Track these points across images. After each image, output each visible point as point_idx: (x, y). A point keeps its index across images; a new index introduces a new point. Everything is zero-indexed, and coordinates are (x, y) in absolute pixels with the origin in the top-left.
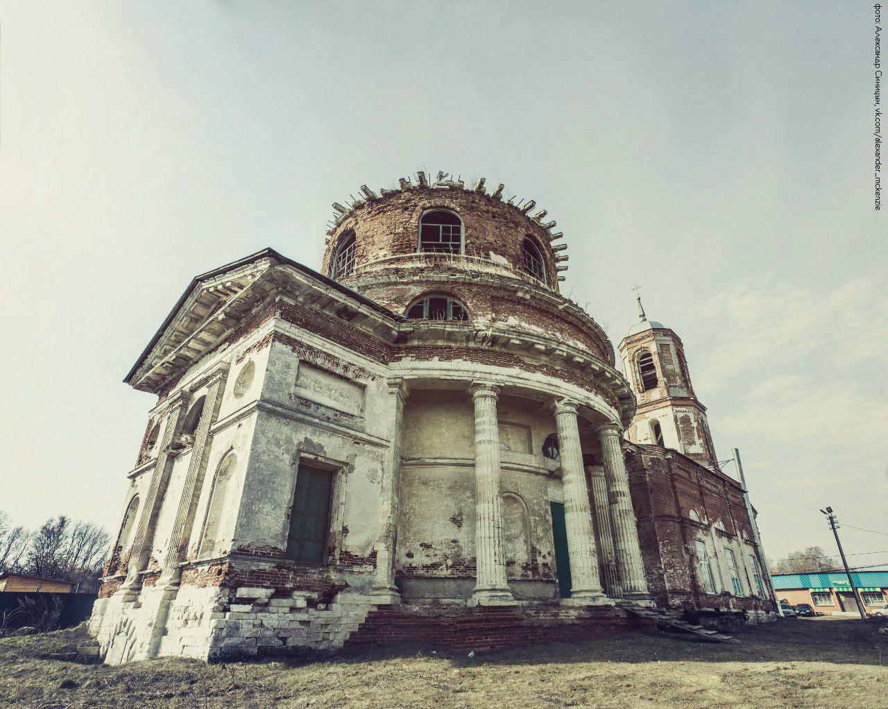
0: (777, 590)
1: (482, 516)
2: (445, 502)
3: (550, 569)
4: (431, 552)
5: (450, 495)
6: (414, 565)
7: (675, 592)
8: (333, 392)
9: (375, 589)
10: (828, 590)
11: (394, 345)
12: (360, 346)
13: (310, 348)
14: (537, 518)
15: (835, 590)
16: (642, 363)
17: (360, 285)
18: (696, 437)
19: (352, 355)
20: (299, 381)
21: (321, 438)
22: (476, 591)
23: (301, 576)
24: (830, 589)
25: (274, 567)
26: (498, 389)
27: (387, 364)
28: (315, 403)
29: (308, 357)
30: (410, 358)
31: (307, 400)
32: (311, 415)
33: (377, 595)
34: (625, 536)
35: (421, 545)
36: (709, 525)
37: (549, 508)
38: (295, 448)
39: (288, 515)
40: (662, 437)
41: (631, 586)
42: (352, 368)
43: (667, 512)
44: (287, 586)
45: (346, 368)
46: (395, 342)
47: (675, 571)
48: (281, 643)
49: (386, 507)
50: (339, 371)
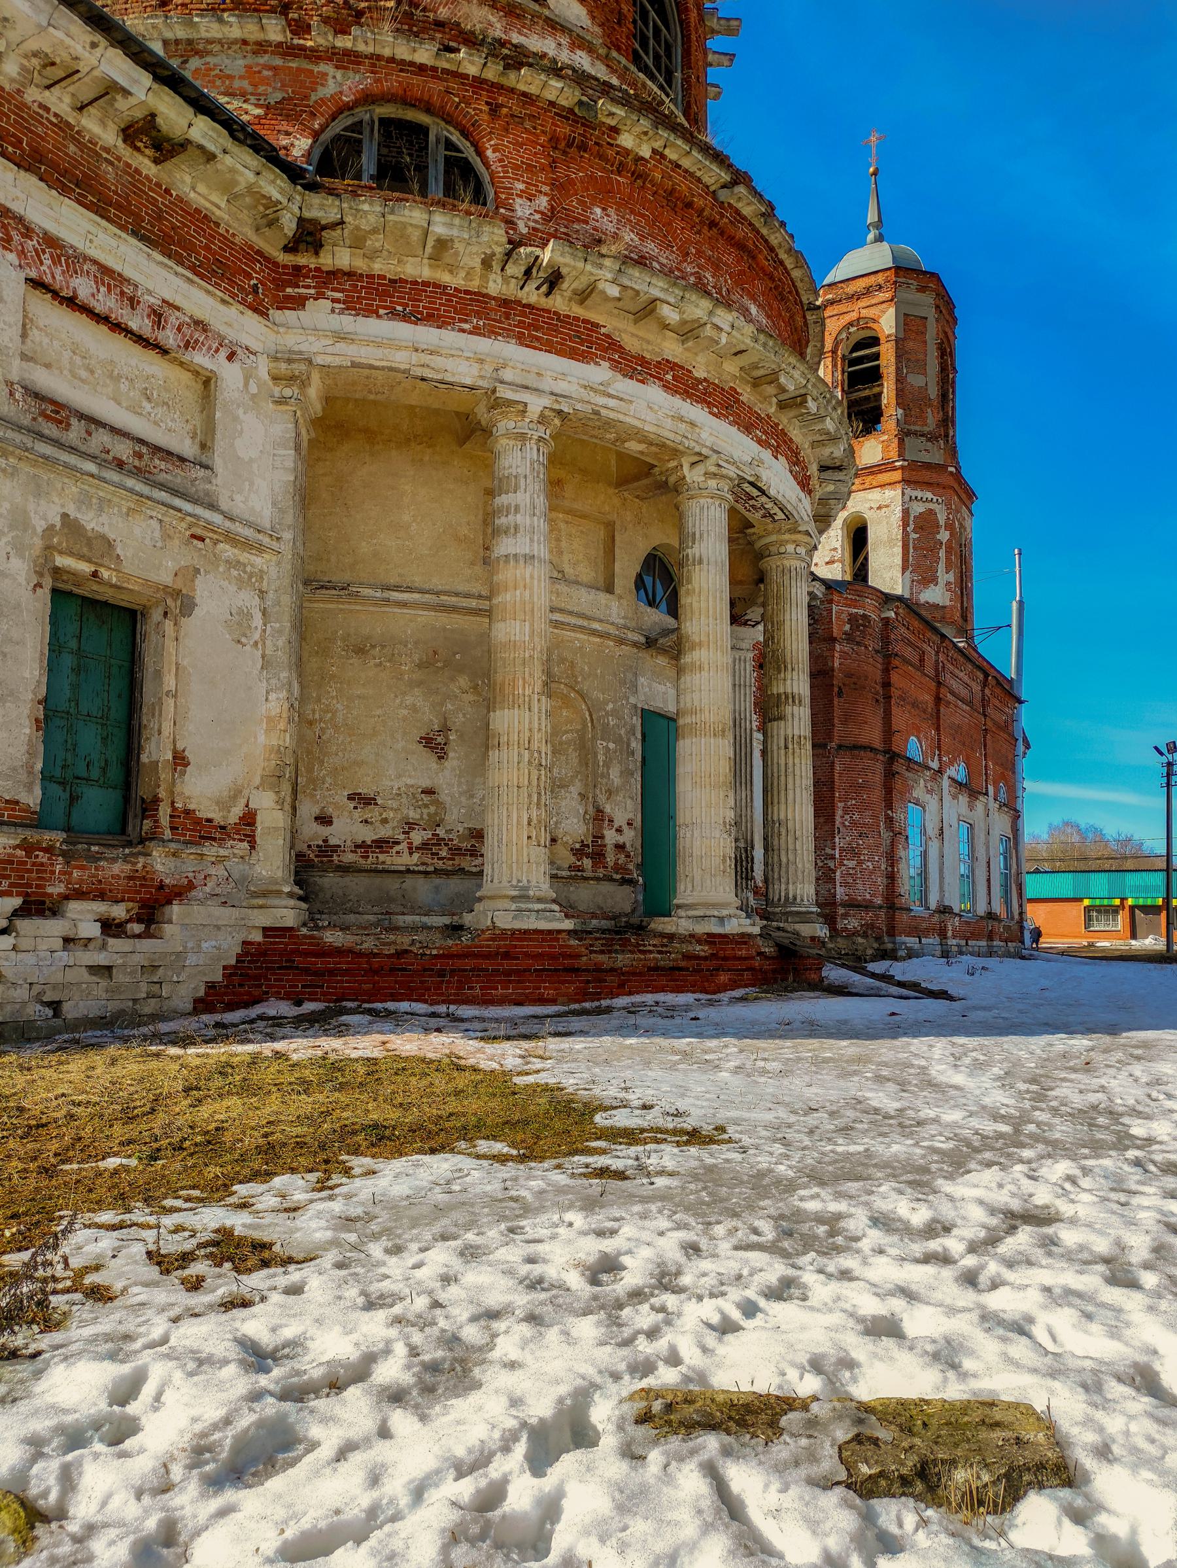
0: (1031, 901)
1: (504, 739)
2: (409, 700)
3: (628, 856)
4: (372, 813)
5: (420, 684)
6: (332, 841)
7: (853, 904)
8: (124, 386)
9: (255, 895)
10: (1117, 902)
11: (283, 258)
12: (190, 248)
13: (51, 241)
14: (612, 746)
15: (1130, 902)
16: (853, 362)
17: (169, 35)
18: (941, 567)
19: (172, 277)
20: (28, 341)
21: (104, 518)
22: (480, 899)
23: (82, 868)
24: (1123, 900)
25: (15, 847)
26: (557, 422)
27: (264, 314)
28: (82, 416)
29: (47, 269)
30: (327, 304)
31: (58, 406)
32: (73, 449)
33: (261, 907)
34: (790, 793)
35: (351, 798)
36: (940, 772)
37: (637, 721)
38: (38, 542)
39: (37, 720)
40: (866, 559)
41: (787, 898)
42: (173, 319)
43: (863, 740)
44: (50, 890)
45: (157, 317)
46: (286, 249)
47: (860, 863)
48: (50, 1013)
49: (276, 704)
50: (138, 322)
